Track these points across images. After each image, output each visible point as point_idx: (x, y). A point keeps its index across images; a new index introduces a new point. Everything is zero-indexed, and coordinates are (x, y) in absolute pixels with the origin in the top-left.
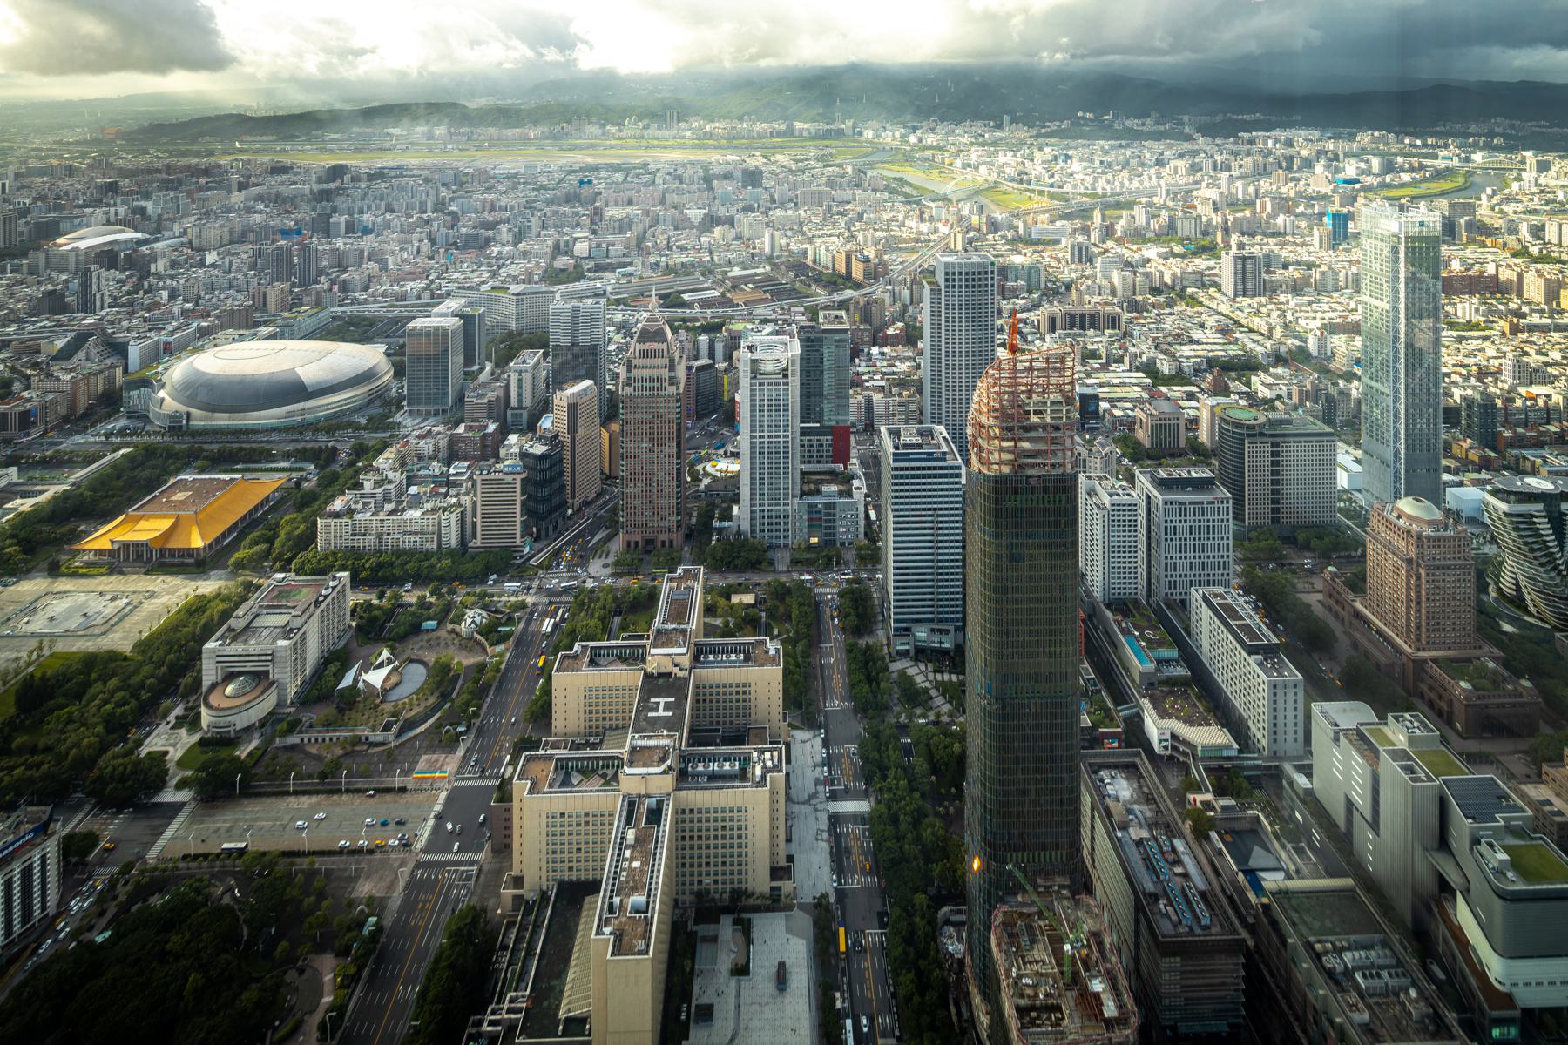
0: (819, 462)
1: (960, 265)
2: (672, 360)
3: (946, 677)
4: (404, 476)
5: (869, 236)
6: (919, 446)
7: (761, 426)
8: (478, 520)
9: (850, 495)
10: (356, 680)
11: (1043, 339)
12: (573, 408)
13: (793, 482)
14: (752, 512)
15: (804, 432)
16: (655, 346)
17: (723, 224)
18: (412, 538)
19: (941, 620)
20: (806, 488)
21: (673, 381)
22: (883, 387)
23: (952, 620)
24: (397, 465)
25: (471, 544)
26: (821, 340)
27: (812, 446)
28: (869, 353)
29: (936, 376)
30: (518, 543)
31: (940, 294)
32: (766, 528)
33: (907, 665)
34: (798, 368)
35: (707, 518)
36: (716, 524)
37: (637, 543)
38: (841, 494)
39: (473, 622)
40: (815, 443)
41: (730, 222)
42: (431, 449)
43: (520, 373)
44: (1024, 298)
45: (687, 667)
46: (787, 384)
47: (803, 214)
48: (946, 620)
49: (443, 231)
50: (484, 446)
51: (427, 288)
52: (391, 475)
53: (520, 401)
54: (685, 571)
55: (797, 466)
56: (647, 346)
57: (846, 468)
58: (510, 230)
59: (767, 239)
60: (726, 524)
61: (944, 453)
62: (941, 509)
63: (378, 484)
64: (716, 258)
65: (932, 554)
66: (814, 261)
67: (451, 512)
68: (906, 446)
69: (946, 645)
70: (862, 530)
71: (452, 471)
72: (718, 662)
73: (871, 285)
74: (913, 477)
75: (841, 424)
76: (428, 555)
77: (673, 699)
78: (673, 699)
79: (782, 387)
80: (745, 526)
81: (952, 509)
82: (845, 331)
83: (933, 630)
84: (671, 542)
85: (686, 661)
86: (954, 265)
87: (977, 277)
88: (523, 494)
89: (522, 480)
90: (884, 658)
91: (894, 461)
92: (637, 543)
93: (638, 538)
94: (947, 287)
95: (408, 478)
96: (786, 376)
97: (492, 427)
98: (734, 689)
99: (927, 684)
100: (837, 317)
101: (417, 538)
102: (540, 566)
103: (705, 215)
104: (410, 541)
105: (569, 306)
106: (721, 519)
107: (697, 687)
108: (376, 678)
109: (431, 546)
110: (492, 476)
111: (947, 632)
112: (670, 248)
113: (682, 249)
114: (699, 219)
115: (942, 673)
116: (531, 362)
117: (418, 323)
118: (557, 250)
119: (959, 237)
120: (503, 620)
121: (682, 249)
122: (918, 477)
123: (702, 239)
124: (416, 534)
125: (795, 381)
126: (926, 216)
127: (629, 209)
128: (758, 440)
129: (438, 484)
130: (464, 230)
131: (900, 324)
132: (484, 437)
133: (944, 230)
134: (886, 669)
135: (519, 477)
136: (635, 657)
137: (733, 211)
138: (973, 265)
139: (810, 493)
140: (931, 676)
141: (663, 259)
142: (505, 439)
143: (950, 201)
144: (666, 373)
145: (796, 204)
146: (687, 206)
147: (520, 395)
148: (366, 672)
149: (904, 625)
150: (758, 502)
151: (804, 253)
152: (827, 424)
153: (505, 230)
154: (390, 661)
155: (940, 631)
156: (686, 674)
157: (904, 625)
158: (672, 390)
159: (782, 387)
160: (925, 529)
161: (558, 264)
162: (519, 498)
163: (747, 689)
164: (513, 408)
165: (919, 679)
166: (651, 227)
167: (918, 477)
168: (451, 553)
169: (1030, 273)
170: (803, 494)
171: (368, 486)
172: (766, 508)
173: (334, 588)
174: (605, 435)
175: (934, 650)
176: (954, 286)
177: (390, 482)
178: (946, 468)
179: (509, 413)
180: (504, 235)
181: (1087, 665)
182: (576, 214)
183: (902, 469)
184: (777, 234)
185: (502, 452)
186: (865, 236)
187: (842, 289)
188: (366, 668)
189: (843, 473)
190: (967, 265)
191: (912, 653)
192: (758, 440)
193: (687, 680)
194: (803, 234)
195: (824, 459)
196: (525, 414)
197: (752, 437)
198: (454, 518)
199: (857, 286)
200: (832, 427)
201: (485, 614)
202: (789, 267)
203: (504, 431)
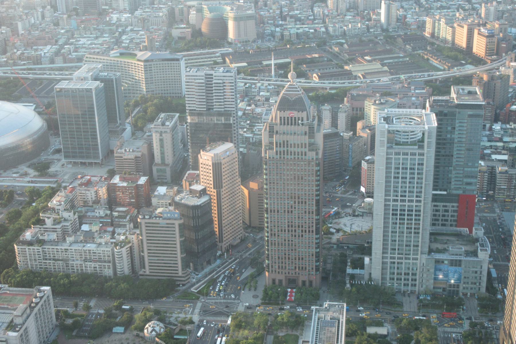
52: (66, 215)
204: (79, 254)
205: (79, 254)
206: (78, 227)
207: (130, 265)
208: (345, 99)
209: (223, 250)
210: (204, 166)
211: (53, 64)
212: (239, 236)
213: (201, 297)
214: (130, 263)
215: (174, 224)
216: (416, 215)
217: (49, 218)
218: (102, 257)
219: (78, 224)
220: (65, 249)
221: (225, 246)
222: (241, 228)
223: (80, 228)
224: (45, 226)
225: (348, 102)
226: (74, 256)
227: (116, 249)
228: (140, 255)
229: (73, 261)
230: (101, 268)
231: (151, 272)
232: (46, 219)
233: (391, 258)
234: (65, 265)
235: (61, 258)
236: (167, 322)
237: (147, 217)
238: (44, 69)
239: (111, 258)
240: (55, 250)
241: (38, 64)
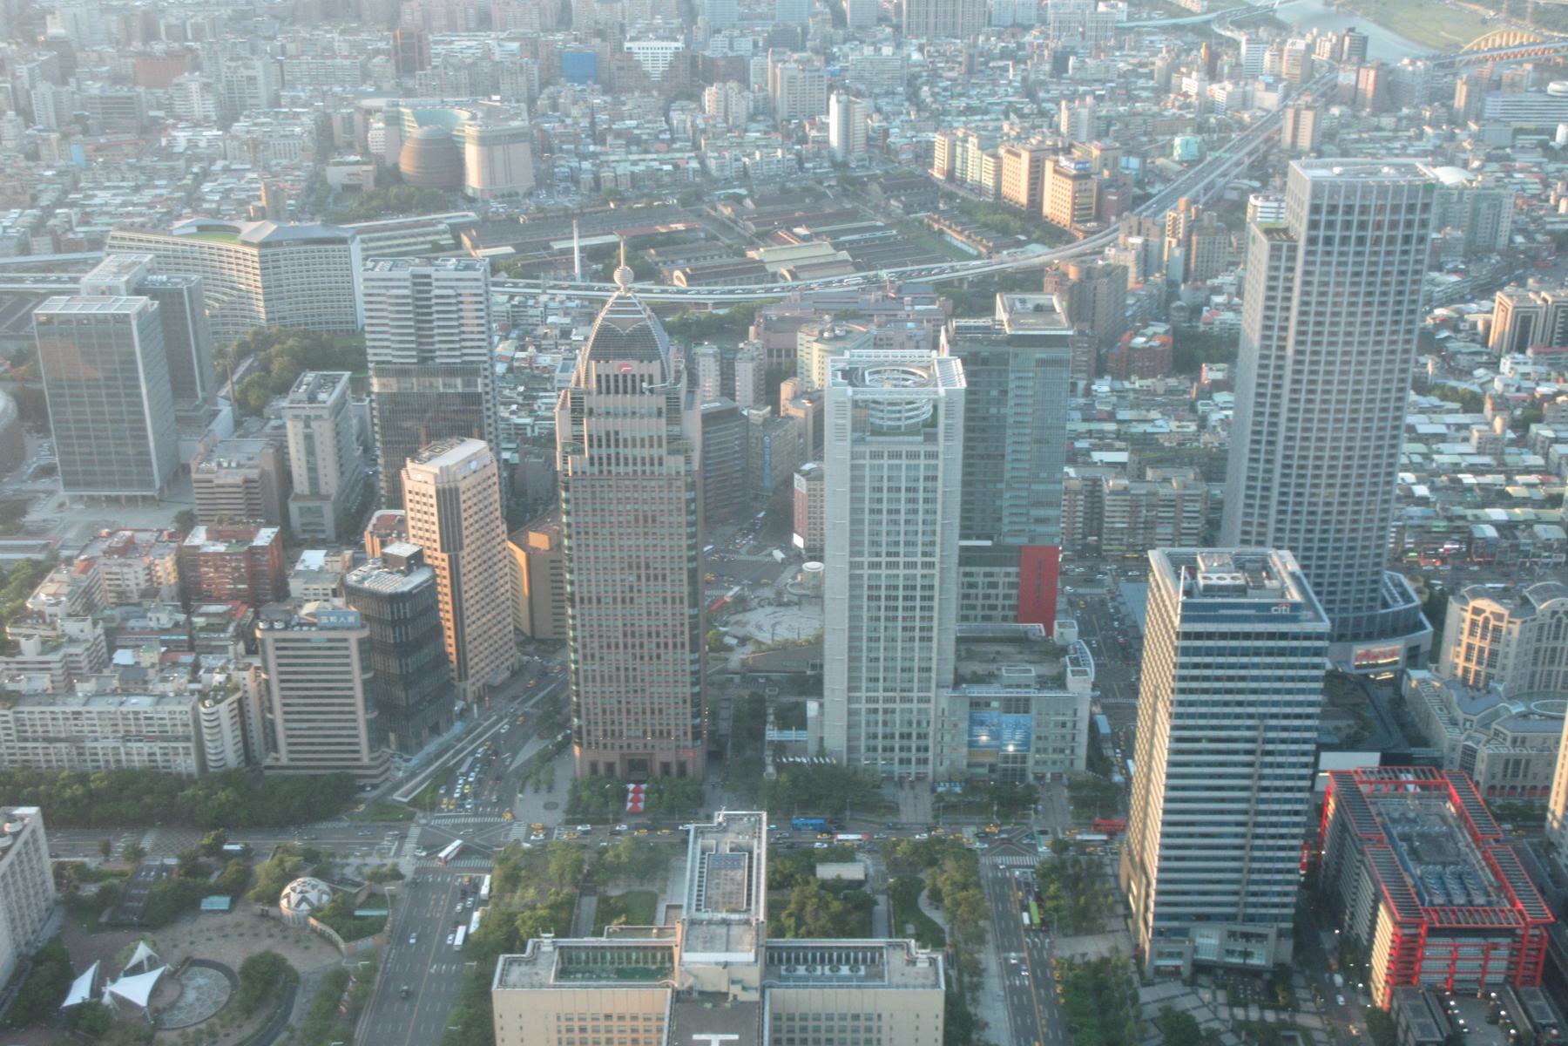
0: (986, 618)
1: (1351, 190)
2: (672, 400)
3: (1254, 1014)
4: (99, 630)
5: (1084, 112)
6: (1241, 590)
7: (874, 543)
8: (278, 717)
9: (1059, 682)
10: (96, 991)
11: (1494, 365)
12: (448, 498)
13: (942, 651)
14: (851, 713)
15: (968, 558)
16: (633, 367)
17: (725, 78)
18: (146, 747)
19: (1251, 919)
20: (971, 667)
21: (676, 444)
22: (1123, 465)
23: (1275, 918)
24: (78, 607)
25: (268, 761)
26: (1003, 360)
27: (994, 585)
28: (1088, 392)
29: (1264, 439)
30: (366, 761)
31: (1292, 258)
32: (880, 743)
33: (472, 930)
34: (959, 422)
35: (751, 720)
36: (772, 734)
37: (610, 766)
38: (1043, 682)
39: (303, 899)
40: (980, 580)
41: (737, 70)
42: (142, 577)
43: (307, 421)
44: (1455, 271)
45: (757, 983)
46: (934, 455)
47: (916, 56)
48: (1263, 918)
49: (44, 88)
50: (253, 575)
51: (37, 228)
52: (72, 627)
53: (314, 481)
54: (729, 819)
55: (947, 625)
56: (615, 367)
57: (1049, 630)
58: (206, 87)
59: (834, 119)
60: (792, 735)
61: (1295, 607)
62: (1274, 716)
63: (48, 646)
64: (712, 164)
65: (1247, 800)
66: (950, 174)
67: (217, 702)
68: (1209, 590)
69: (1255, 961)
70: (1082, 752)
71: (199, 621)
72: (816, 979)
73: (1088, 233)
74: (1221, 652)
75: (1039, 542)
76: (182, 781)
77: (735, 1037)
78: (735, 1037)
79: (922, 462)
80: (836, 739)
81: (1298, 716)
82: (1060, 341)
83: (1232, 934)
84: (682, 767)
85: (754, 976)
86: (1334, 188)
87: (1356, 218)
88: (364, 669)
89: (361, 642)
90: (1129, 982)
91: (1184, 619)
92: (610, 766)
93: (613, 756)
94: (1312, 241)
95: (109, 633)
96: (931, 438)
97: (265, 536)
98: (849, 1023)
99: (1215, 1025)
100: (1039, 309)
101: (156, 747)
102: (415, 803)
103: (677, 55)
104: (138, 754)
105: (404, 273)
106: (784, 725)
107: (776, 1017)
108: (136, 989)
109: (186, 764)
110: (295, 634)
111: (1262, 937)
112: (599, 139)
113: (632, 141)
114: (661, 67)
115: (1245, 1006)
116: (328, 398)
117: (56, 306)
118: (327, 142)
119: (1307, 118)
120: (362, 898)
121: (632, 141)
122: (1233, 652)
123: (676, 117)
124: (152, 739)
125: (950, 450)
126: (1226, 62)
127: (490, 39)
128: (866, 572)
129: (174, 647)
130: (94, 88)
131: (1161, 328)
132: (253, 552)
133: (1270, 100)
134: (1135, 998)
135: (353, 637)
136: (653, 966)
137: (744, 46)
138: (1383, 190)
139: (977, 679)
140: (1224, 1013)
141: (586, 165)
142: (294, 562)
143: (1281, 27)
144: (660, 427)
145: (897, 28)
146: (631, 33)
147: (312, 469)
148: (114, 980)
149: (1175, 924)
150: (863, 694)
151: (924, 154)
152: (1010, 541)
153: (194, 87)
154: (152, 964)
155: (1247, 936)
156: (754, 996)
157: (1175, 924)
158: (675, 463)
159: (922, 462)
160: (1236, 752)
161: (336, 175)
162: (357, 677)
163: (874, 1024)
164: (299, 497)
165: (1201, 1016)
166: (545, 84)
167: (1233, 652)
168: (228, 778)
169: (1476, 212)
170: (959, 680)
171: (29, 648)
172: (880, 706)
173: (16, 835)
174: (520, 556)
175: (1230, 969)
176: (1328, 241)
177: (72, 641)
178: (1296, 637)
179: (294, 508)
180: (196, 98)
181: (1542, 1002)
182: (359, 48)
183: (1199, 636)
184: (862, 105)
185: (295, 586)
186: (1073, 115)
187: (1020, 244)
188: (110, 972)
189: (1045, 641)
190: (1367, 190)
191: (1186, 971)
192: (866, 572)
193: (760, 1005)
194: (920, 106)
195: (999, 613)
196: (329, 512)
197: (853, 565)
198: (224, 709)
199: (1055, 235)
200: (1020, 548)
201: (323, 886)
202: (308, 196)
203: (290, 543)
209: (470, 697)
212: (507, 664)
215: (345, 640)
217: (29, 637)
223: (111, 659)
224: (19, 658)
225: (758, 335)
228: (263, 718)
229: (96, 740)
232: (23, 641)
237: (278, 625)
239: (191, 728)
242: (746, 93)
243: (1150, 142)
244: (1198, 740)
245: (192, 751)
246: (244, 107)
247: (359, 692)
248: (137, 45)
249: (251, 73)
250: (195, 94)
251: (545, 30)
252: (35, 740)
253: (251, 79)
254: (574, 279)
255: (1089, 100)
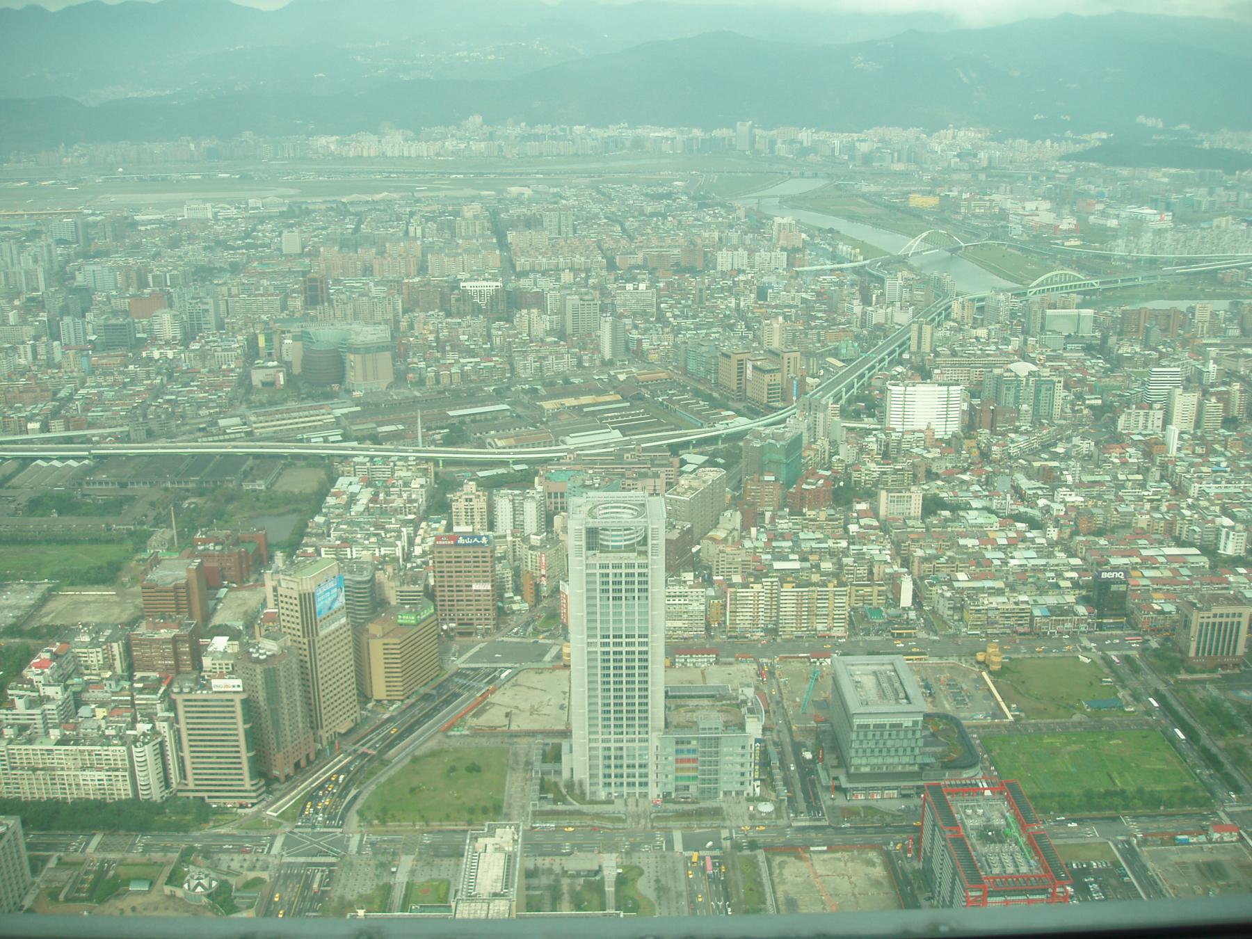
52: (51, 691)
204: (71, 757)
205: (71, 757)
206: (74, 711)
207: (162, 774)
208: (537, 479)
209: (325, 742)
210: (286, 600)
211: (48, 431)
212: (352, 717)
213: (285, 823)
214: (161, 770)
215: (232, 700)
216: (609, 719)
217: (21, 697)
218: (112, 762)
219: (73, 707)
220: (47, 750)
221: (327, 735)
222: (355, 703)
223: (77, 713)
224: (14, 712)
225: (541, 483)
226: (64, 761)
227: (136, 747)
228: (178, 755)
229: (62, 769)
230: (111, 780)
231: (196, 785)
232: (16, 699)
233: (604, 741)
234: (48, 777)
235: (41, 766)
236: (224, 867)
237: (186, 690)
238: (31, 441)
239: (127, 762)
240: (31, 752)
241: (21, 433)
242: (543, 316)
243: (823, 346)
244: (218, 757)
245: (128, 778)
246: (200, 330)
247: (242, 738)
248: (132, 291)
249: (206, 307)
250: (166, 323)
251: (408, 276)
252: (22, 769)
253: (207, 311)
254: (417, 446)
255: (781, 318)
